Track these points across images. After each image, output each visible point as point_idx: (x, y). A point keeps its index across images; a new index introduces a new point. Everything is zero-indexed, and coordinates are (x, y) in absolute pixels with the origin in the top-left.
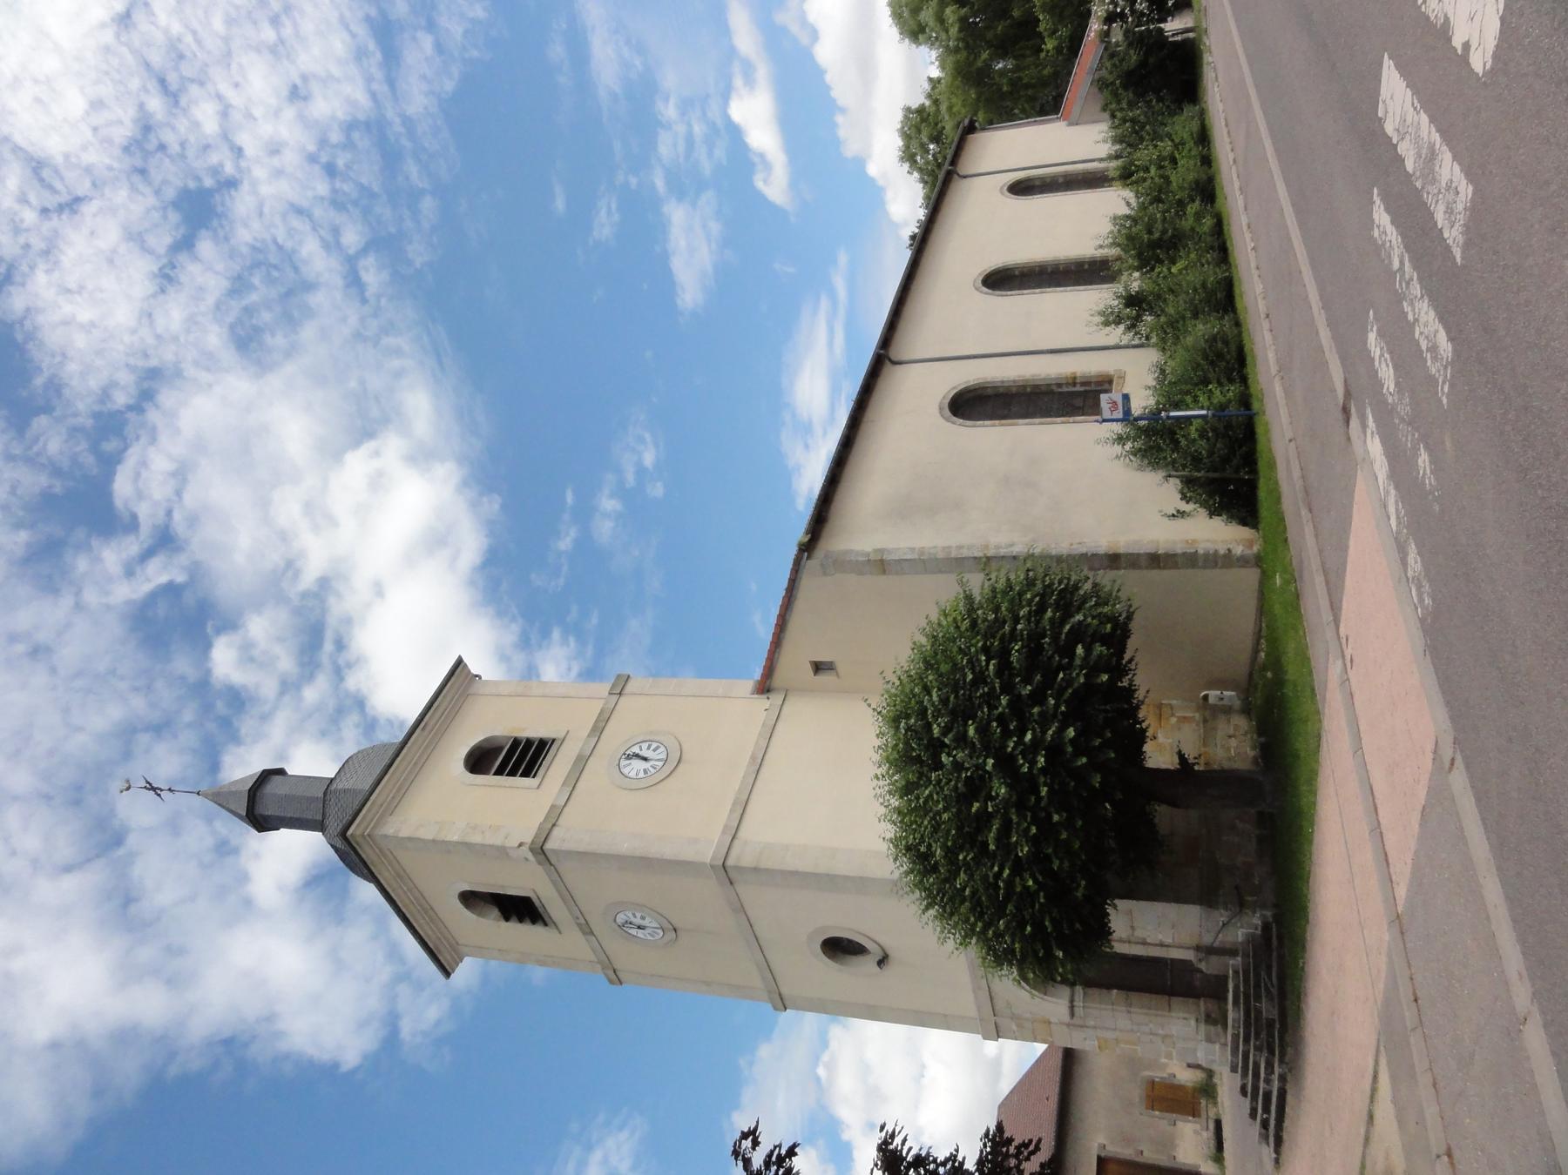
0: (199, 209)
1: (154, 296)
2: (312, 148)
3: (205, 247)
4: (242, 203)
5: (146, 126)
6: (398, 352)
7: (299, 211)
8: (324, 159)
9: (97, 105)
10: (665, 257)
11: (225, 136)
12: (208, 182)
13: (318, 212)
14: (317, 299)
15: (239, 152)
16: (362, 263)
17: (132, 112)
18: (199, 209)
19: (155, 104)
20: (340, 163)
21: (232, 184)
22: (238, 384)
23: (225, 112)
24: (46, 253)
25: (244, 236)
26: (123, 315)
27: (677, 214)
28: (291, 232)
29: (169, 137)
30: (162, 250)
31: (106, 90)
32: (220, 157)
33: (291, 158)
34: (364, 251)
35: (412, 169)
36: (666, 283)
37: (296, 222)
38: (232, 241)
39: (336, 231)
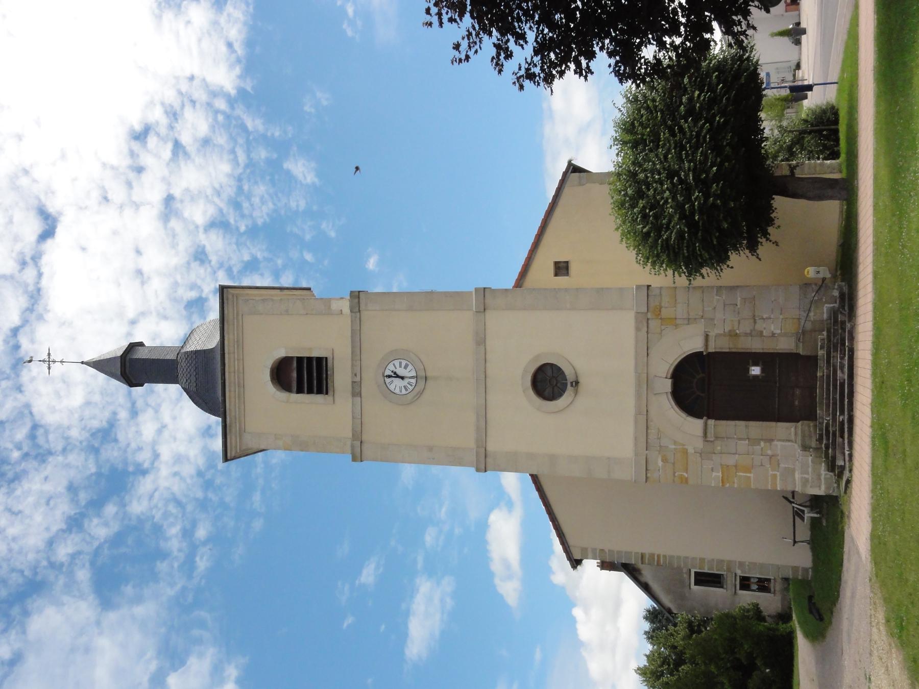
0: (193, 102)
1: (63, 531)
2: (202, 468)
3: (110, 509)
4: (145, 485)
5: (112, 424)
6: (202, 624)
7: (179, 503)
8: (209, 476)
9: (88, 403)
10: (407, 614)
11: (154, 443)
12: (131, 469)
13: (189, 508)
14: (162, 566)
15: (156, 456)
16: (203, 550)
17: (107, 414)
18: (193, 102)
19: (123, 415)
20: (218, 481)
21: (144, 472)
22: (83, 609)
23: (160, 431)
24: (12, 481)
25: (137, 508)
26: (35, 540)
27: (424, 586)
28: (166, 515)
29: (121, 436)
30: (83, 503)
31: (97, 398)
32: (144, 457)
33: (188, 470)
34: (205, 543)
35: (257, 497)
36: (403, 636)
37: (172, 508)
38: (127, 508)
39: (194, 524)
